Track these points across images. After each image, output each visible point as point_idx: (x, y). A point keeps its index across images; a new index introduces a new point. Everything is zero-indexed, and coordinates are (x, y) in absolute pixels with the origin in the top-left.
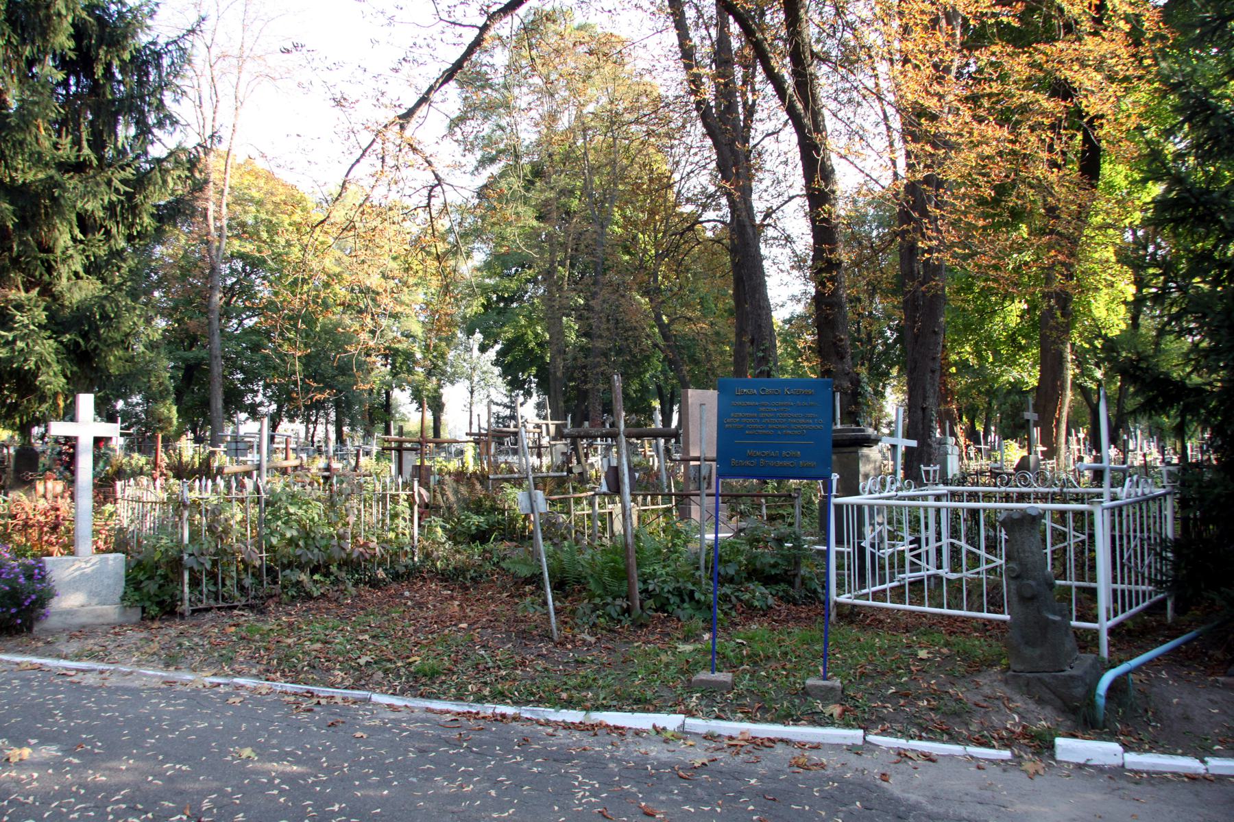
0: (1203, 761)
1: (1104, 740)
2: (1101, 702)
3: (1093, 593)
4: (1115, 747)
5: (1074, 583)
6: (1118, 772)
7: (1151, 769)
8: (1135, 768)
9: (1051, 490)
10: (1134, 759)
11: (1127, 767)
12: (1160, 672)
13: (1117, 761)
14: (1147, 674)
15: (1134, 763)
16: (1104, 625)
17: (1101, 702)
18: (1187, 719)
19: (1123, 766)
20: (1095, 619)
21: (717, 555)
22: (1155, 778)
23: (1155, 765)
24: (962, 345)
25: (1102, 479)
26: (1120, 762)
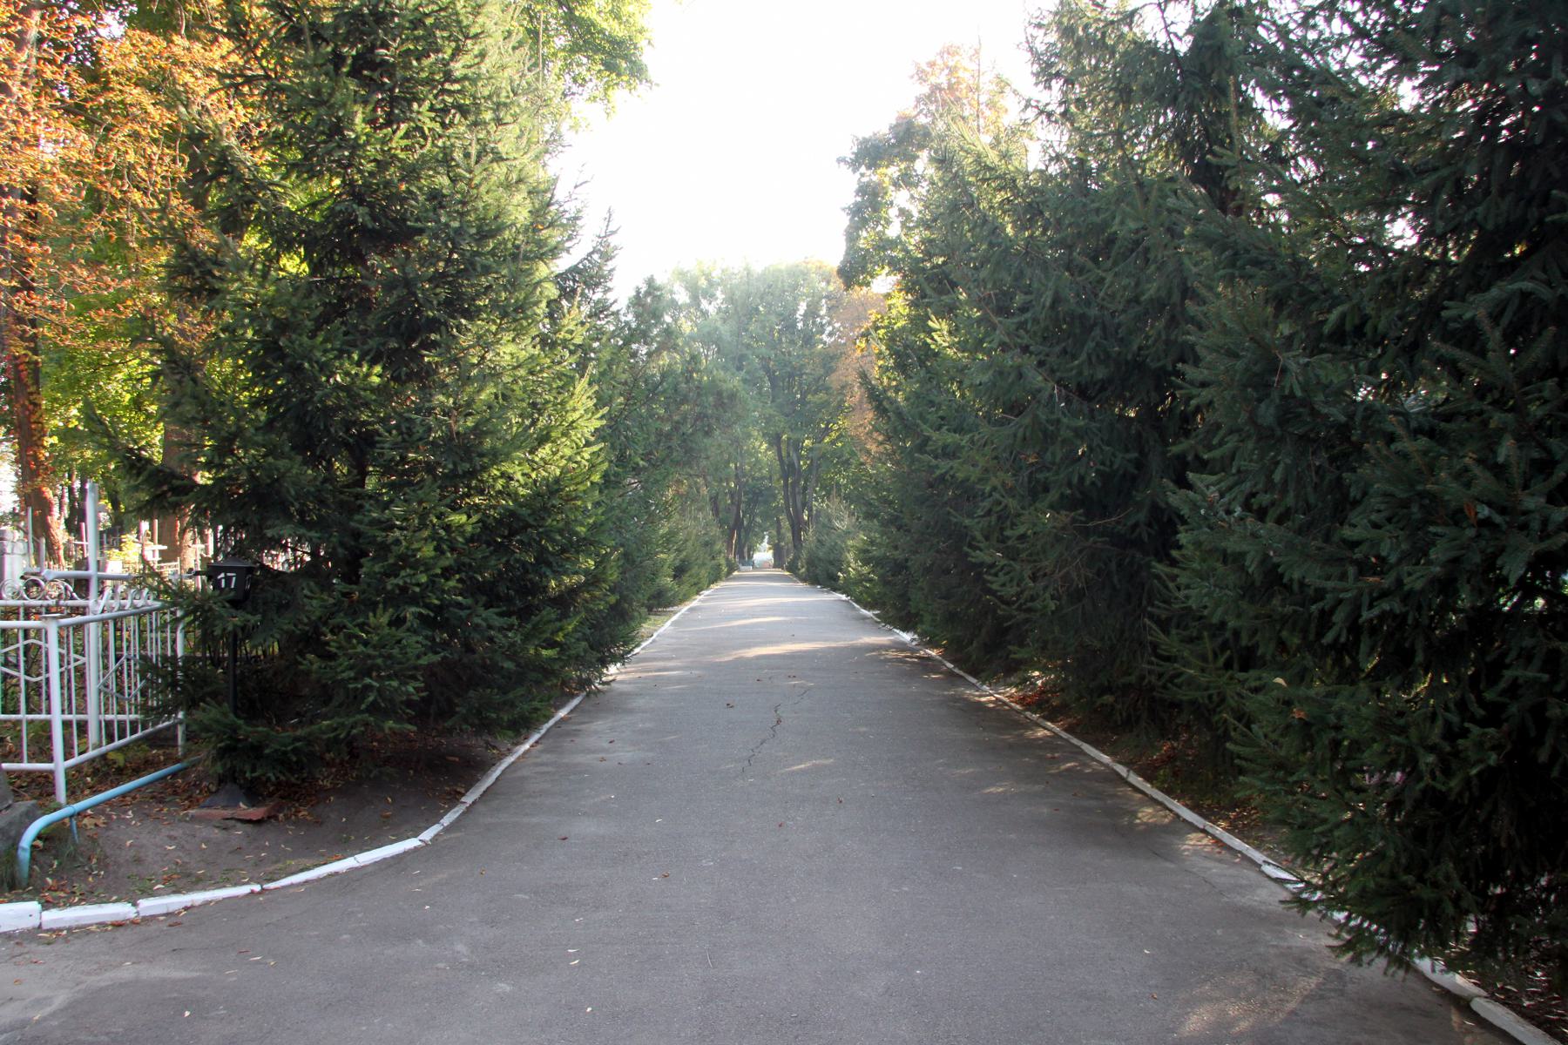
0: (135, 905)
1: (24, 900)
2: (24, 855)
3: (47, 725)
4: (34, 906)
5: (23, 716)
6: (34, 934)
7: (74, 924)
8: (54, 926)
9: (45, 603)
10: (54, 917)
11: (45, 927)
12: (125, 812)
13: (34, 922)
14: (109, 817)
15: (55, 921)
16: (59, 766)
17: (24, 855)
18: (138, 861)
19: (40, 926)
20: (51, 760)
21: (1317, 985)
22: (80, 932)
23: (78, 919)
24: (67, 406)
25: (88, 590)
26: (37, 923)
